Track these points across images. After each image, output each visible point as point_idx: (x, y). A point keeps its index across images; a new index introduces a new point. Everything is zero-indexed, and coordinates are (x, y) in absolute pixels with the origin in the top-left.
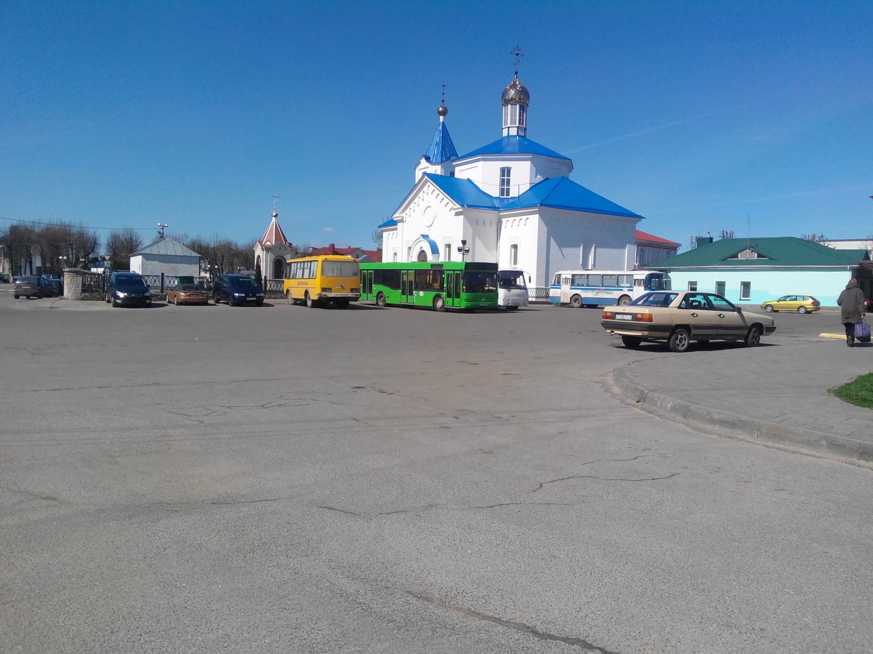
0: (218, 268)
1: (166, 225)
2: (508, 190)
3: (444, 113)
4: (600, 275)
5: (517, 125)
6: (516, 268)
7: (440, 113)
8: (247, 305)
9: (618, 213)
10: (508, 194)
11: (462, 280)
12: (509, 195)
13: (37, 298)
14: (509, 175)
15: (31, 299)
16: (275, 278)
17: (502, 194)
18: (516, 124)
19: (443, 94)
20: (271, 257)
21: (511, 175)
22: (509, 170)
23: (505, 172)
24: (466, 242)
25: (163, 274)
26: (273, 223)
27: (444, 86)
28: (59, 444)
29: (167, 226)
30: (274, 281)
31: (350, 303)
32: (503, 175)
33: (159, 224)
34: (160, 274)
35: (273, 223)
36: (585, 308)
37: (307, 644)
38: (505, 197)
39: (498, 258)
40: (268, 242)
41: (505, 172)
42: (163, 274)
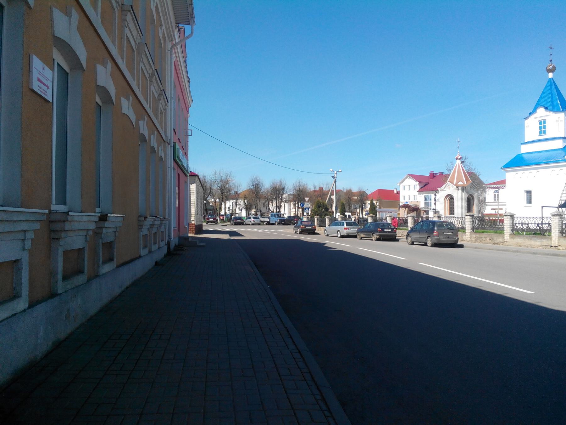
0: (205, 203)
1: (340, 171)
3: (552, 71)
7: (549, 71)
8: (24, 207)
9: (538, 163)
13: (307, 233)
15: (423, 242)
16: (450, 215)
19: (551, 55)
20: (465, 195)
21: (547, 128)
26: (456, 165)
27: (551, 48)
28: (299, 368)
29: (341, 172)
30: (449, 217)
31: (385, 230)
33: (331, 170)
35: (456, 165)
40: (460, 182)
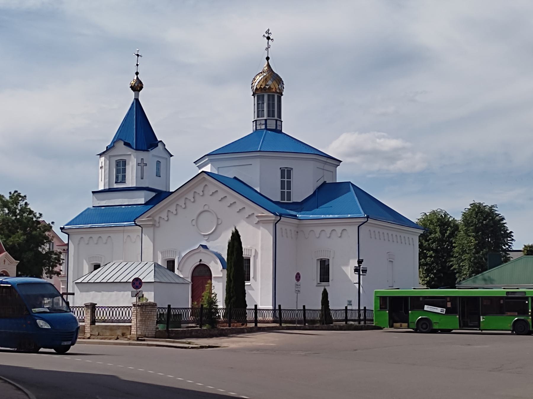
2: (289, 194)
4: (394, 328)
5: (265, 118)
6: (217, 344)
10: (289, 198)
11: (334, 323)
12: (290, 200)
13: (53, 351)
14: (289, 177)
17: (283, 198)
18: (264, 117)
22: (289, 171)
23: (286, 173)
24: (366, 271)
25: (169, 306)
32: (283, 176)
34: (167, 307)
36: (439, 333)
37: (464, 238)
38: (286, 201)
39: (256, 303)
41: (286, 173)
42: (169, 306)
